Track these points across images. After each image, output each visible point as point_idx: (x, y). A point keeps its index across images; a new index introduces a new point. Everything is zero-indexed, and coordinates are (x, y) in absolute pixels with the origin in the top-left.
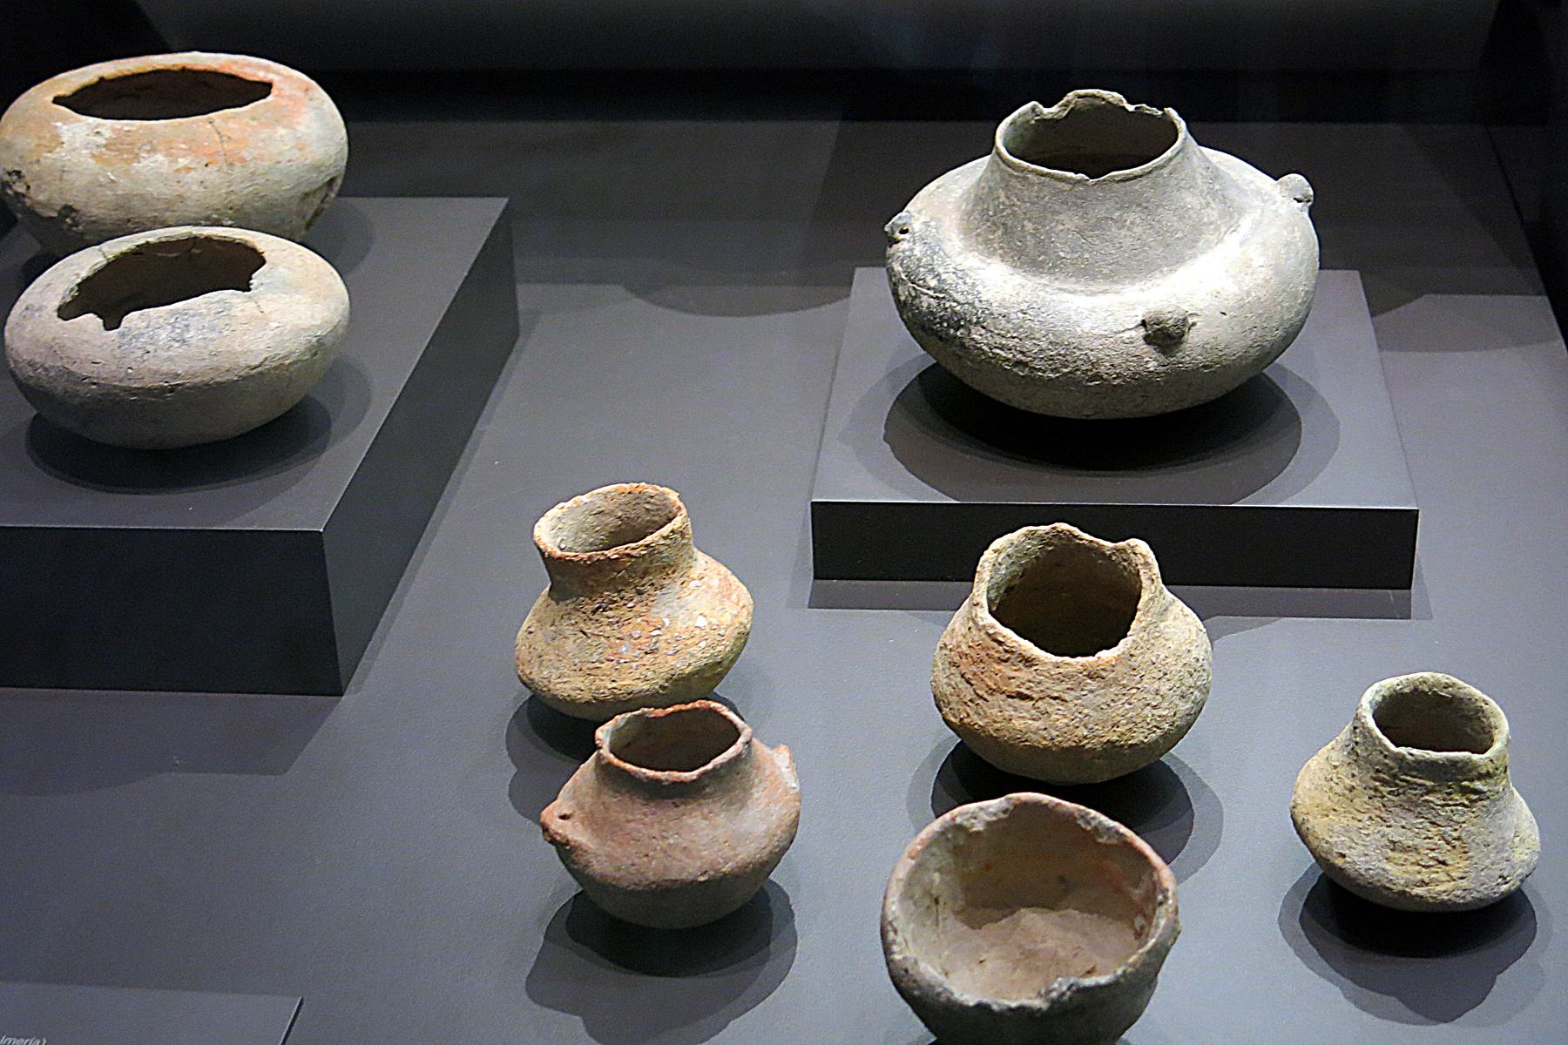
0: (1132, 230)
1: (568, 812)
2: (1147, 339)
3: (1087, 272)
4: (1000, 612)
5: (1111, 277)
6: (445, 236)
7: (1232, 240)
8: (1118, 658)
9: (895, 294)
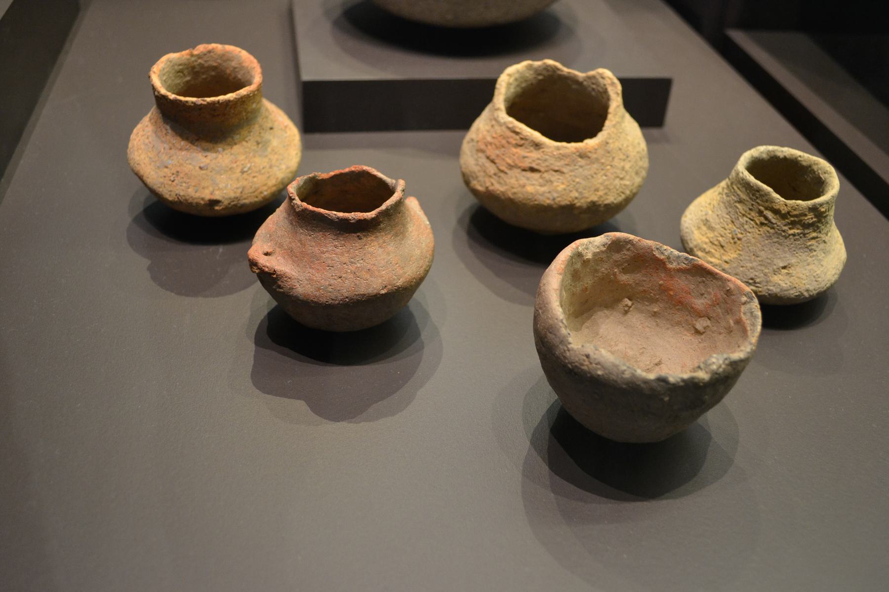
1: (269, 251)
4: (513, 110)
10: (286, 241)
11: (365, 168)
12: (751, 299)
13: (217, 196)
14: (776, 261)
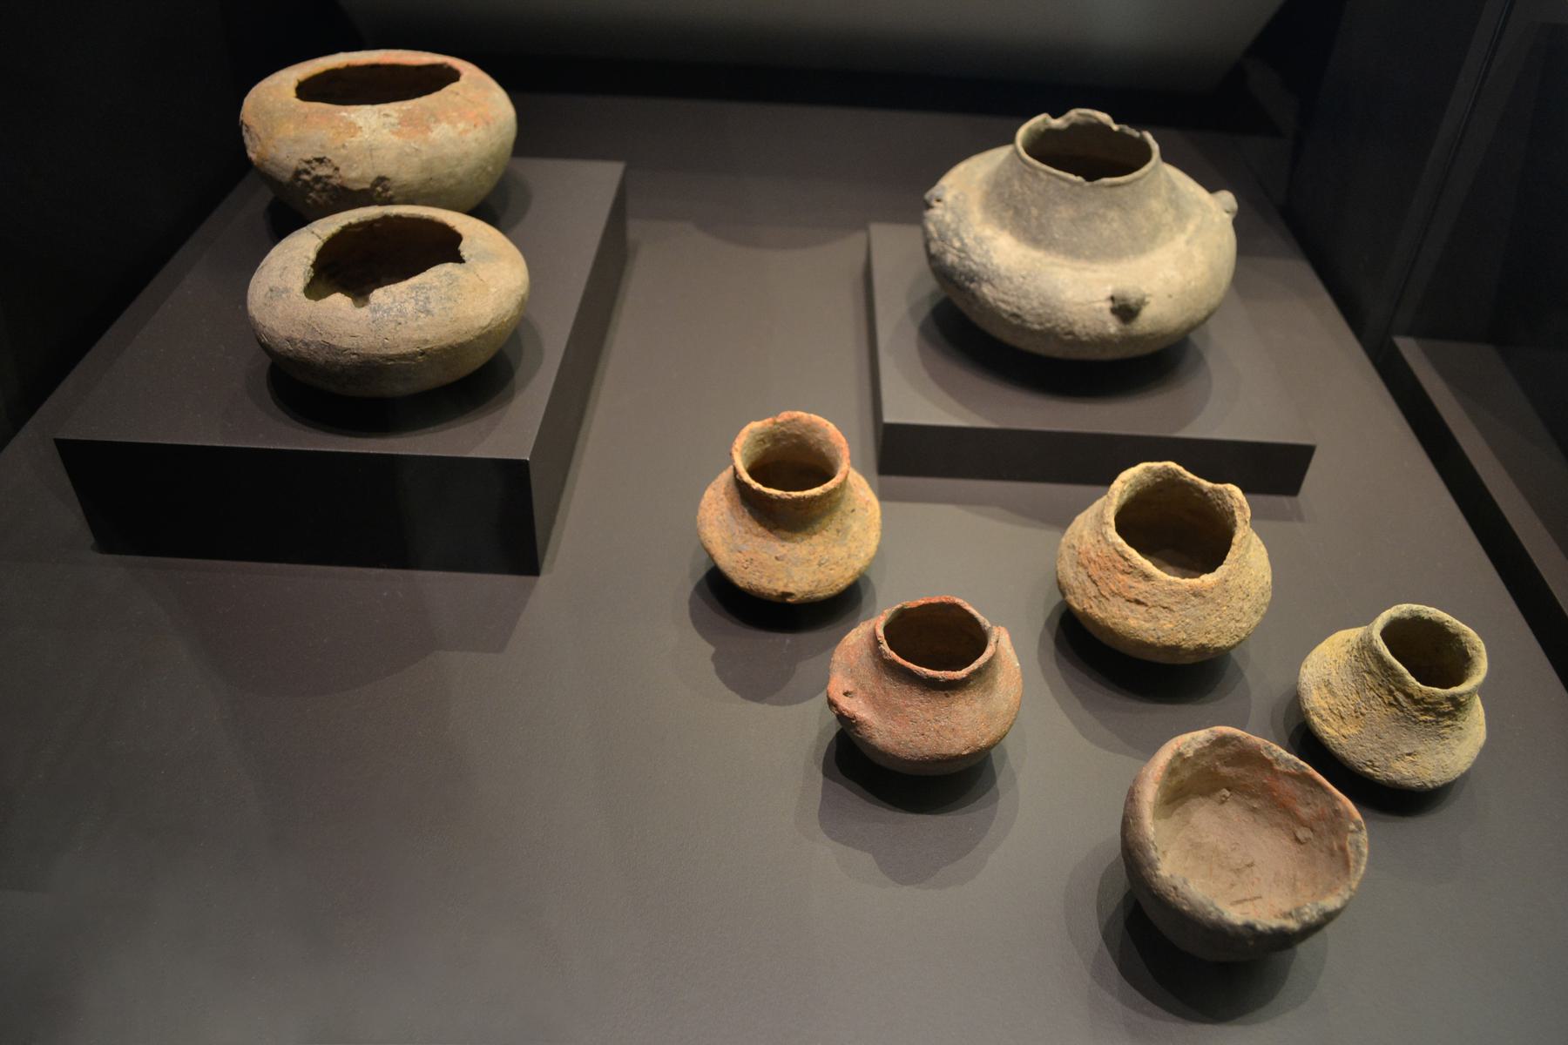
0: (1112, 224)
2: (1114, 311)
3: (1073, 251)
5: (1092, 258)
6: (586, 188)
7: (1181, 240)
8: (1218, 584)
9: (927, 247)
10: (869, 683)
11: (958, 601)
12: (1360, 829)
13: (791, 588)
14: (1400, 746)
